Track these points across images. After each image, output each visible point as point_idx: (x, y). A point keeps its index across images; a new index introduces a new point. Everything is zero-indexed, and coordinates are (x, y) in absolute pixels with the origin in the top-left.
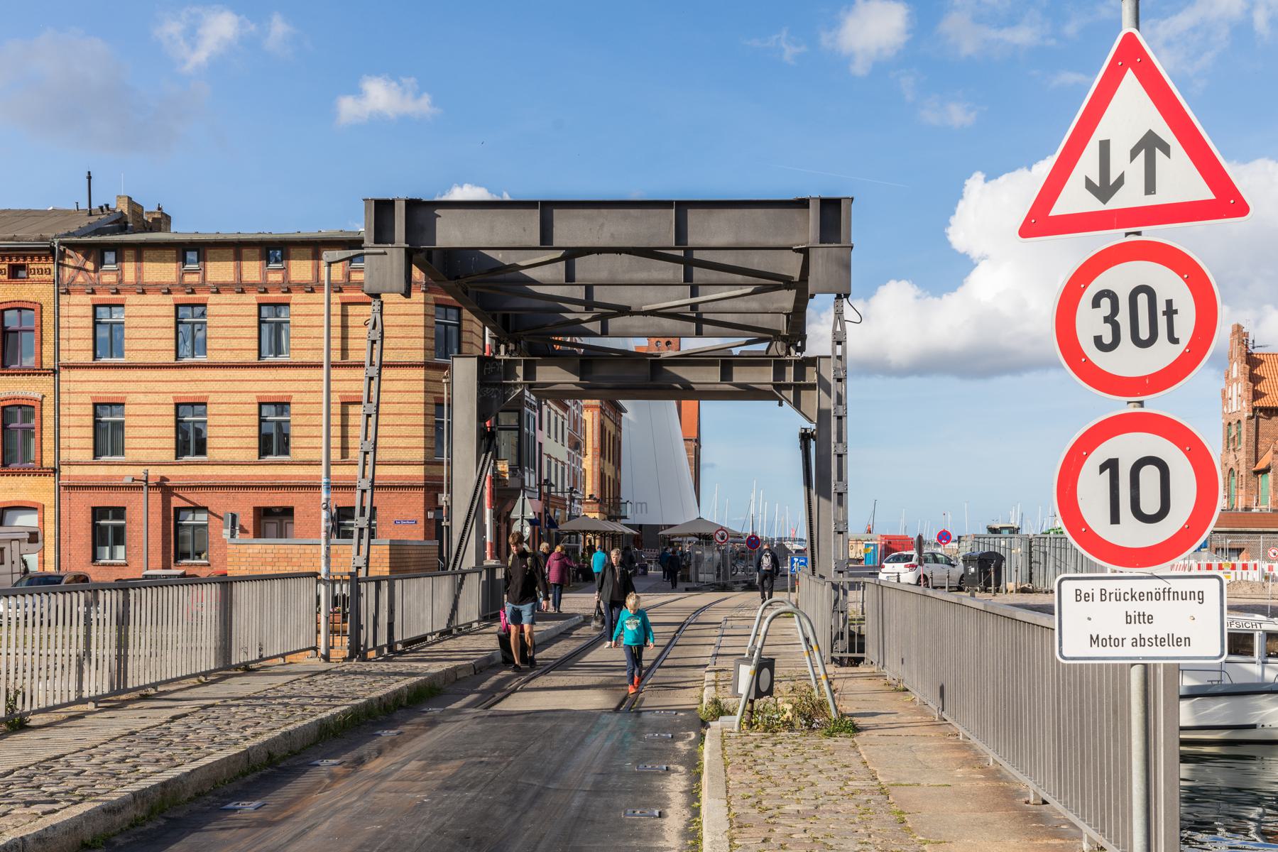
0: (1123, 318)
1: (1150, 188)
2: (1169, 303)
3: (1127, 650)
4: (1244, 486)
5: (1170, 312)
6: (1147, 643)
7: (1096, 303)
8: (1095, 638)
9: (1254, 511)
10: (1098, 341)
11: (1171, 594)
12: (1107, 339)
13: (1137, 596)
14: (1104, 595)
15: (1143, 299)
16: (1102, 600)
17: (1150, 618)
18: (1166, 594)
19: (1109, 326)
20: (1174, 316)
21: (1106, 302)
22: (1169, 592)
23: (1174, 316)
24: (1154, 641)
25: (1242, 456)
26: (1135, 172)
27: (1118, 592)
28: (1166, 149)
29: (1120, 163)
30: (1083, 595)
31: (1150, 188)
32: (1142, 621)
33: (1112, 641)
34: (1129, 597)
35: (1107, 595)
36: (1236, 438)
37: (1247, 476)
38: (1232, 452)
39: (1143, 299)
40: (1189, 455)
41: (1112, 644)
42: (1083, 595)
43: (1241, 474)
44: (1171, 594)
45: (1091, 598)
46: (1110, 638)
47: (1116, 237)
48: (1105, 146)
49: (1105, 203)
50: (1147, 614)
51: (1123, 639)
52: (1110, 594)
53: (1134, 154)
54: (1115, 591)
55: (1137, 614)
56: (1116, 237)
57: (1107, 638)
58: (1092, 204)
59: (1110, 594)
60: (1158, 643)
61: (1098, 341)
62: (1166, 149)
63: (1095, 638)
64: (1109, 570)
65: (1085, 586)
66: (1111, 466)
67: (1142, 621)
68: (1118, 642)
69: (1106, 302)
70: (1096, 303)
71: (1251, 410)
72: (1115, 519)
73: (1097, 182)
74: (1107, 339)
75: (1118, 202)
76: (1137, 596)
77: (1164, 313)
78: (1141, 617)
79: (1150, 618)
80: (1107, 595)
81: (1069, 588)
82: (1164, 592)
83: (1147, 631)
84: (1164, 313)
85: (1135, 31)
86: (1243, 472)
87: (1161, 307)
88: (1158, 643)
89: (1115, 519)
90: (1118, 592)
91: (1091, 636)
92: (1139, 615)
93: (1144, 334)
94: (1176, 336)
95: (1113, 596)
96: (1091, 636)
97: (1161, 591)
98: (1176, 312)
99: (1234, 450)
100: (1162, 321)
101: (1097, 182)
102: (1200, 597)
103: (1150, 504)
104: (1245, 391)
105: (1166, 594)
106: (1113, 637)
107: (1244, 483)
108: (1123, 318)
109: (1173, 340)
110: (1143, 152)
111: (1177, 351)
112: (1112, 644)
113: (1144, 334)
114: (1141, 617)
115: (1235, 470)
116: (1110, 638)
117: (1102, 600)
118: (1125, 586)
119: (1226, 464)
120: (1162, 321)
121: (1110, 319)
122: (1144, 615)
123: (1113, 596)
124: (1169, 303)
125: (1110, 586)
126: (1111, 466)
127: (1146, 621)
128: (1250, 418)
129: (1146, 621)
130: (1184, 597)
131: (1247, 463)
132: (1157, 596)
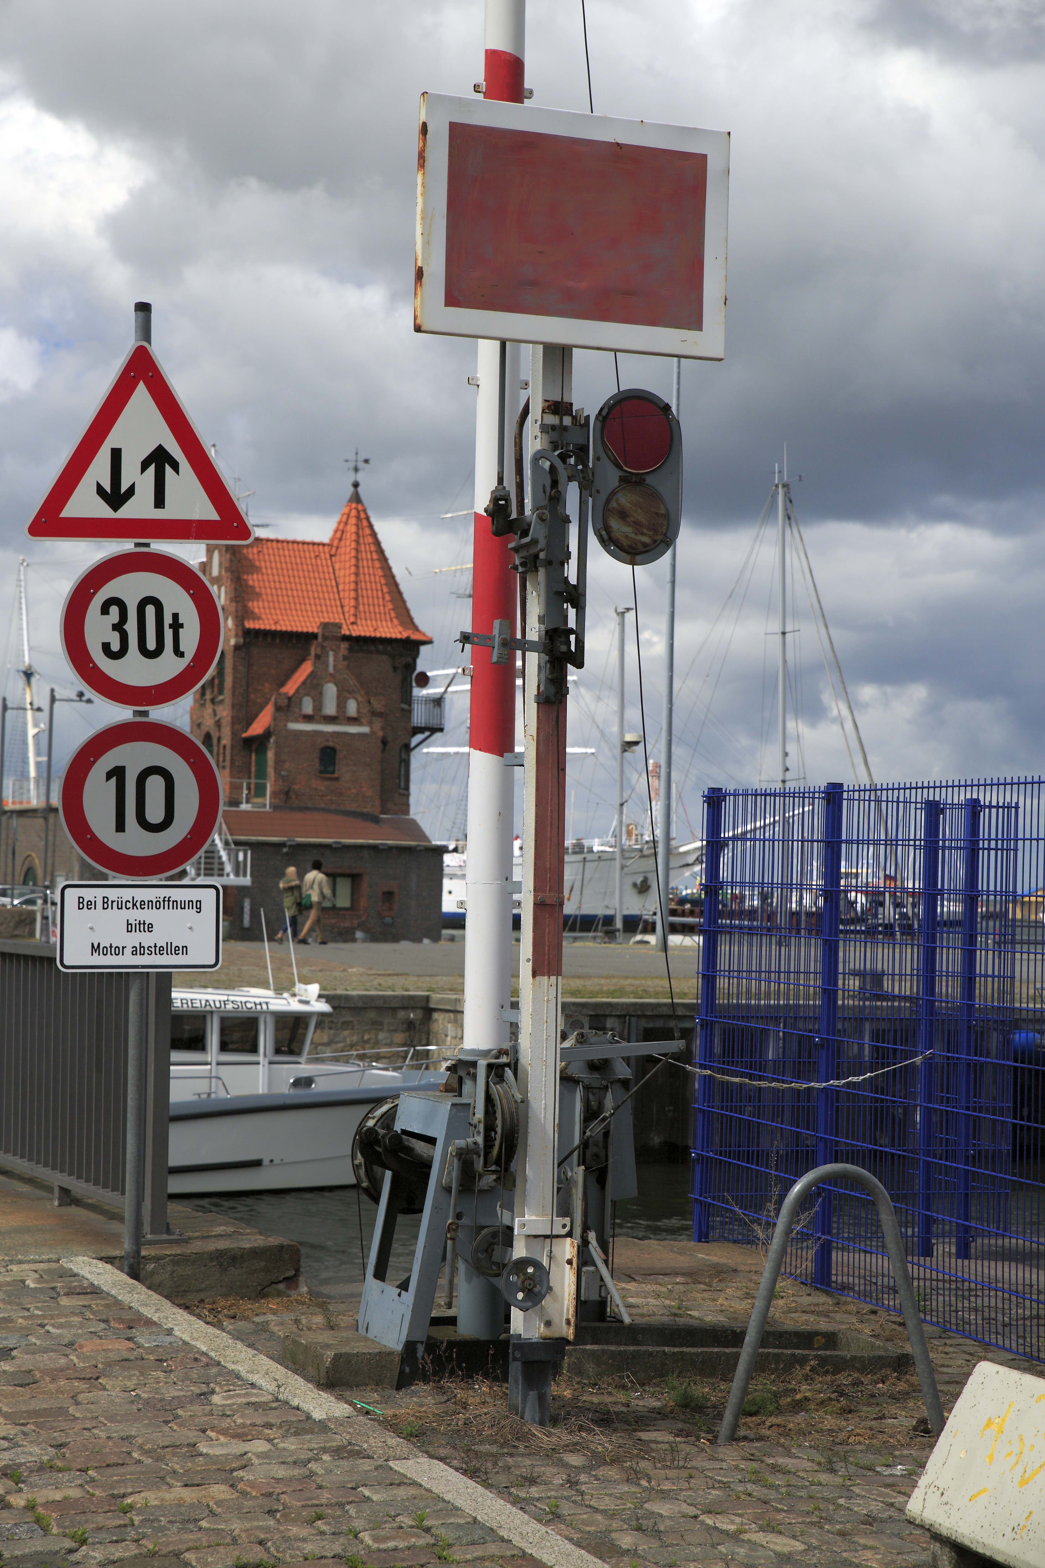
0: (131, 627)
1: (159, 502)
2: (175, 616)
3: (127, 959)
4: (228, 764)
5: (176, 626)
6: (146, 951)
7: (105, 610)
8: (96, 946)
9: (244, 807)
10: (106, 647)
11: (171, 903)
12: (115, 647)
13: (138, 904)
14: (106, 903)
15: (150, 610)
16: (104, 908)
17: (151, 926)
18: (166, 903)
19: (117, 635)
20: (181, 630)
21: (114, 610)
22: (169, 901)
23: (181, 630)
24: (153, 950)
25: (225, 712)
26: (146, 483)
27: (120, 900)
28: (175, 466)
29: (130, 474)
30: (85, 903)
31: (159, 502)
32: (142, 929)
33: (113, 949)
34: (130, 905)
35: (110, 903)
36: (216, 681)
37: (233, 747)
38: (209, 705)
39: (150, 610)
40: (192, 766)
41: (113, 952)
42: (85, 903)
43: (223, 742)
44: (171, 903)
45: (93, 906)
46: (111, 947)
47: (127, 546)
48: (116, 454)
49: (115, 509)
50: (147, 923)
51: (123, 948)
52: (112, 902)
53: (145, 466)
54: (116, 899)
55: (137, 922)
56: (127, 546)
57: (108, 946)
58: (102, 510)
59: (112, 902)
60: (157, 952)
61: (106, 647)
62: (175, 466)
63: (96, 946)
64: (110, 877)
65: (88, 894)
66: (118, 773)
67: (142, 929)
68: (119, 951)
69: (114, 610)
70: (105, 610)
71: (240, 633)
72: (120, 827)
73: (108, 488)
74: (115, 647)
75: (128, 511)
76: (138, 904)
77: (171, 626)
78: (142, 926)
79: (151, 926)
80: (110, 903)
81: (72, 895)
82: (164, 901)
83: (147, 939)
84: (171, 626)
85: (145, 344)
86: (226, 741)
87: (168, 620)
88: (157, 952)
89: (120, 827)
90: (120, 900)
91: (93, 944)
92: (140, 924)
93: (151, 645)
94: (182, 649)
95: (115, 904)
96: (93, 944)
97: (161, 900)
98: (182, 626)
99: (213, 701)
100: (168, 634)
101: (108, 488)
102: (198, 906)
103: (155, 815)
104: (231, 600)
105: (166, 903)
106: (114, 946)
107: (228, 758)
108: (131, 627)
109: (181, 655)
110: (153, 466)
111: (181, 664)
112: (113, 952)
113: (151, 645)
114: (142, 926)
115: (215, 735)
116: (111, 947)
117: (104, 908)
118: (127, 894)
119: (199, 725)
120: (168, 634)
121: (119, 627)
122: (144, 924)
123: (115, 904)
124: (175, 616)
125: (113, 894)
126: (118, 773)
127: (146, 929)
128: (237, 648)
129: (146, 929)
130: (183, 905)
131: (233, 724)
132: (156, 905)
